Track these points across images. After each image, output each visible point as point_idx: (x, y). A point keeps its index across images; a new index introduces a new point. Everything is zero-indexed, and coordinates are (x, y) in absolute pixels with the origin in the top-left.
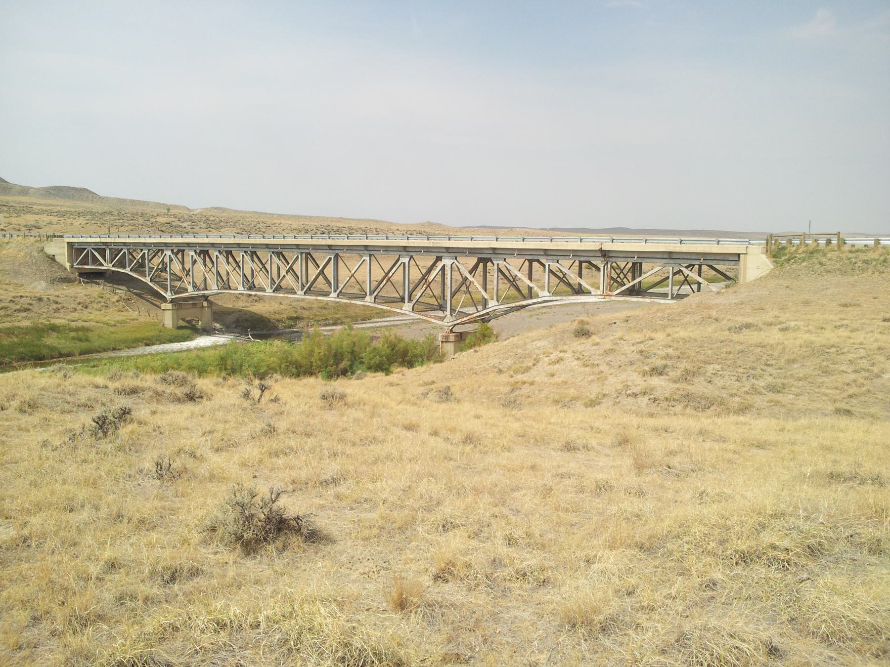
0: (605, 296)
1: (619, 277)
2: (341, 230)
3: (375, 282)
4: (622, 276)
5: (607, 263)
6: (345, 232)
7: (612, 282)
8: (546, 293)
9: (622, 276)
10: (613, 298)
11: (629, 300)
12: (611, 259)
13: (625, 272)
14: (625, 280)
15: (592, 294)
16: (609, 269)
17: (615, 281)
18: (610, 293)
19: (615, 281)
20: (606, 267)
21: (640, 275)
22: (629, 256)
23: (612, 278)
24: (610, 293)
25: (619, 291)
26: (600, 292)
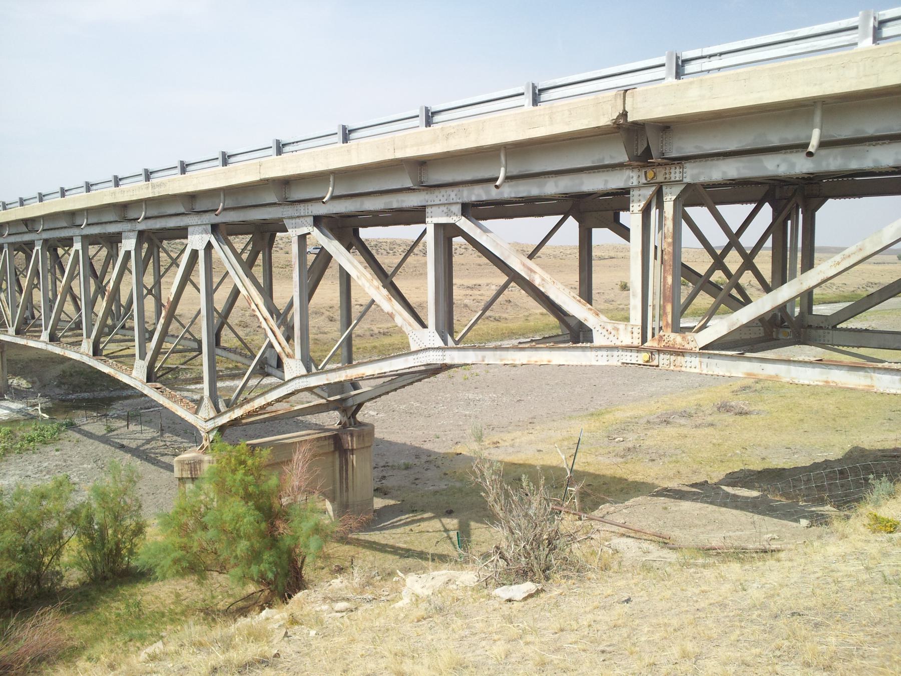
0: (652, 352)
1: (719, 262)
2: (380, 245)
3: (358, 306)
4: (733, 261)
5: (659, 195)
6: (385, 247)
7: (686, 291)
8: (430, 337)
9: (733, 261)
10: (693, 365)
11: (775, 379)
12: (675, 174)
13: (748, 240)
14: (747, 279)
15: (599, 339)
16: (669, 224)
17: (703, 283)
18: (677, 339)
19: (703, 283)
20: (654, 213)
21: (808, 264)
22: (775, 140)
23: (687, 272)
24: (677, 339)
25: (719, 327)
26: (629, 335)
